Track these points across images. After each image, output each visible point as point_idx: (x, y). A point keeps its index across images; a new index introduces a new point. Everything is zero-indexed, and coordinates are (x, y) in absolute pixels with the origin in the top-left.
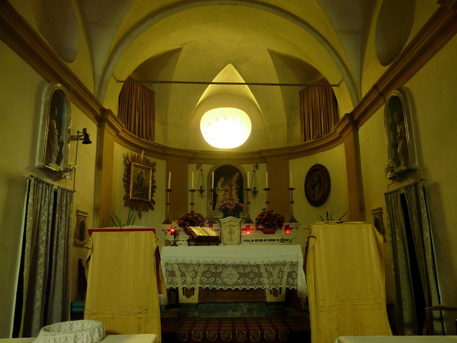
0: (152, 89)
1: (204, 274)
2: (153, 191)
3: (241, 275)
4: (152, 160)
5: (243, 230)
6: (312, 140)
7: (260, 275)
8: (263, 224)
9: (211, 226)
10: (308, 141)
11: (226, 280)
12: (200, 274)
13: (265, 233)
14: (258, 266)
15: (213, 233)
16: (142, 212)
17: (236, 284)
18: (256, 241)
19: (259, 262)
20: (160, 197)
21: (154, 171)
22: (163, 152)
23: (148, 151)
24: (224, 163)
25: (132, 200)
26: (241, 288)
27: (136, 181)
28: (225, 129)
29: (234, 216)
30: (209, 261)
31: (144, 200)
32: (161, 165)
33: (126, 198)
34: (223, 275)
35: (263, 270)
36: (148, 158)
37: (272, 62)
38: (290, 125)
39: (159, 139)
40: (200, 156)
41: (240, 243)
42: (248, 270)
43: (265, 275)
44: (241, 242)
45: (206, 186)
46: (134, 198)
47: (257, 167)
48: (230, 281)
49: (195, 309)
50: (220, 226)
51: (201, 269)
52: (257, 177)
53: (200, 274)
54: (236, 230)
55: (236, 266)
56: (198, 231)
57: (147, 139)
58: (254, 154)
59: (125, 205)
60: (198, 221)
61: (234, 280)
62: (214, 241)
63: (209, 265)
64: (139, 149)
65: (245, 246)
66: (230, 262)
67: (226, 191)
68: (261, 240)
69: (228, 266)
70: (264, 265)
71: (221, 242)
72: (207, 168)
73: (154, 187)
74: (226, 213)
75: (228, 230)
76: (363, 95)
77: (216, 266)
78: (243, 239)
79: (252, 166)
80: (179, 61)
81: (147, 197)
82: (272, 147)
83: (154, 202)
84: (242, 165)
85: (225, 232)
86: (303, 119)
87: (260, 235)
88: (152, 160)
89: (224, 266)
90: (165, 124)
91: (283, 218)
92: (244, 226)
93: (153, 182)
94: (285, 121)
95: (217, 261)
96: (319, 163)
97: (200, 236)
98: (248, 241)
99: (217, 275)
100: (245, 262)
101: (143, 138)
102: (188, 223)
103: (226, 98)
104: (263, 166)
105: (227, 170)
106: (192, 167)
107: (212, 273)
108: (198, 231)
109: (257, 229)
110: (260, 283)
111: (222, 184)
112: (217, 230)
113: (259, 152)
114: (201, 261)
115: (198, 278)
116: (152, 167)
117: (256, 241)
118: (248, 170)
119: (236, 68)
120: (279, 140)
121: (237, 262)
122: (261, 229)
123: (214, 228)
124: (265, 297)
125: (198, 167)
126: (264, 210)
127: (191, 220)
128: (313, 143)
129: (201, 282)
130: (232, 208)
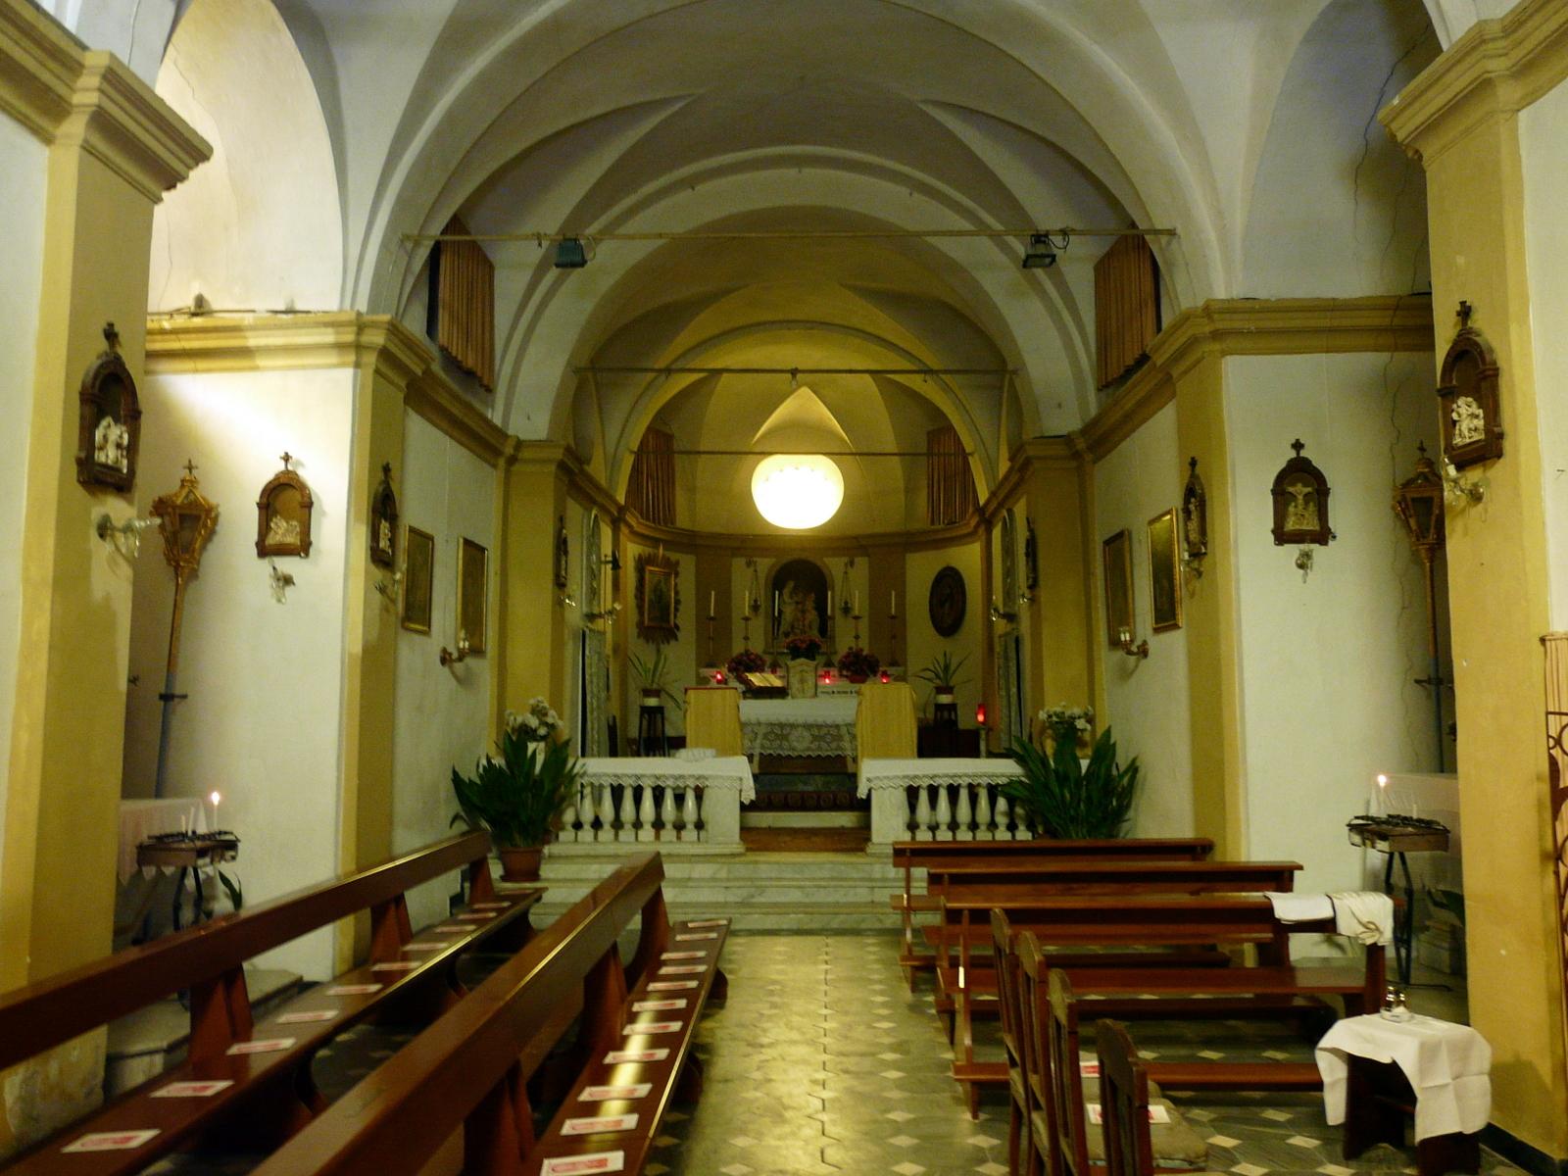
0: (669, 432)
1: (765, 736)
2: (676, 610)
3: (815, 738)
4: (674, 556)
5: (821, 676)
6: (942, 526)
7: (840, 738)
8: (848, 670)
9: (774, 672)
10: (936, 527)
11: (795, 744)
12: (760, 737)
13: (852, 682)
14: (837, 726)
15: (777, 683)
16: (662, 646)
17: (808, 749)
18: (839, 692)
19: (839, 721)
20: (686, 619)
21: (677, 574)
22: (692, 542)
23: (668, 545)
24: (796, 556)
25: (649, 627)
26: (813, 754)
27: (653, 597)
28: (797, 494)
29: (807, 657)
30: (773, 719)
31: (664, 625)
32: (687, 564)
33: (640, 624)
34: (792, 738)
35: (844, 730)
36: (668, 554)
37: (875, 389)
38: (910, 490)
39: (683, 521)
40: (754, 542)
41: (816, 695)
42: (824, 731)
43: (847, 737)
44: (816, 695)
45: (763, 598)
46: (652, 624)
47: (852, 563)
48: (801, 745)
49: (690, 925)
50: (788, 671)
51: (762, 730)
52: (851, 584)
53: (760, 737)
54: (811, 678)
55: (808, 727)
56: (756, 679)
57: (666, 525)
58: (843, 540)
59: (639, 636)
60: (756, 666)
61: (806, 744)
62: (779, 693)
63: (772, 724)
64: (655, 542)
65: (823, 700)
66: (801, 721)
67: (797, 603)
68: (846, 692)
69: (798, 726)
70: (846, 725)
71: (787, 694)
72: (765, 565)
73: (677, 602)
74: (796, 652)
75: (798, 677)
76: (1001, 476)
77: (782, 726)
78: (819, 690)
79: (845, 559)
80: (718, 388)
81: (668, 621)
82: (878, 529)
83: (677, 627)
84: (825, 559)
85: (794, 681)
86: (931, 487)
87: (845, 684)
88: (674, 556)
89: (793, 726)
90: (692, 490)
91: (877, 661)
92: (821, 672)
93: (677, 593)
94: (901, 484)
95: (783, 720)
96: (953, 565)
97: (761, 687)
98: (828, 693)
99: (785, 737)
100: (820, 721)
101: (659, 523)
102: (742, 668)
103: (801, 439)
104: (862, 562)
105: (799, 568)
106: (738, 563)
107: (776, 734)
108: (756, 679)
109: (841, 675)
110: (839, 748)
111: (791, 593)
112: (781, 677)
113: (856, 538)
114: (763, 719)
115: (758, 741)
116: (672, 568)
117: (839, 692)
118: (835, 566)
119: (815, 392)
120: (891, 521)
121: (810, 720)
122: (847, 677)
123: (778, 674)
124: (846, 766)
125: (749, 564)
126: (851, 648)
127: (744, 664)
128: (943, 530)
129: (762, 747)
130: (804, 646)
